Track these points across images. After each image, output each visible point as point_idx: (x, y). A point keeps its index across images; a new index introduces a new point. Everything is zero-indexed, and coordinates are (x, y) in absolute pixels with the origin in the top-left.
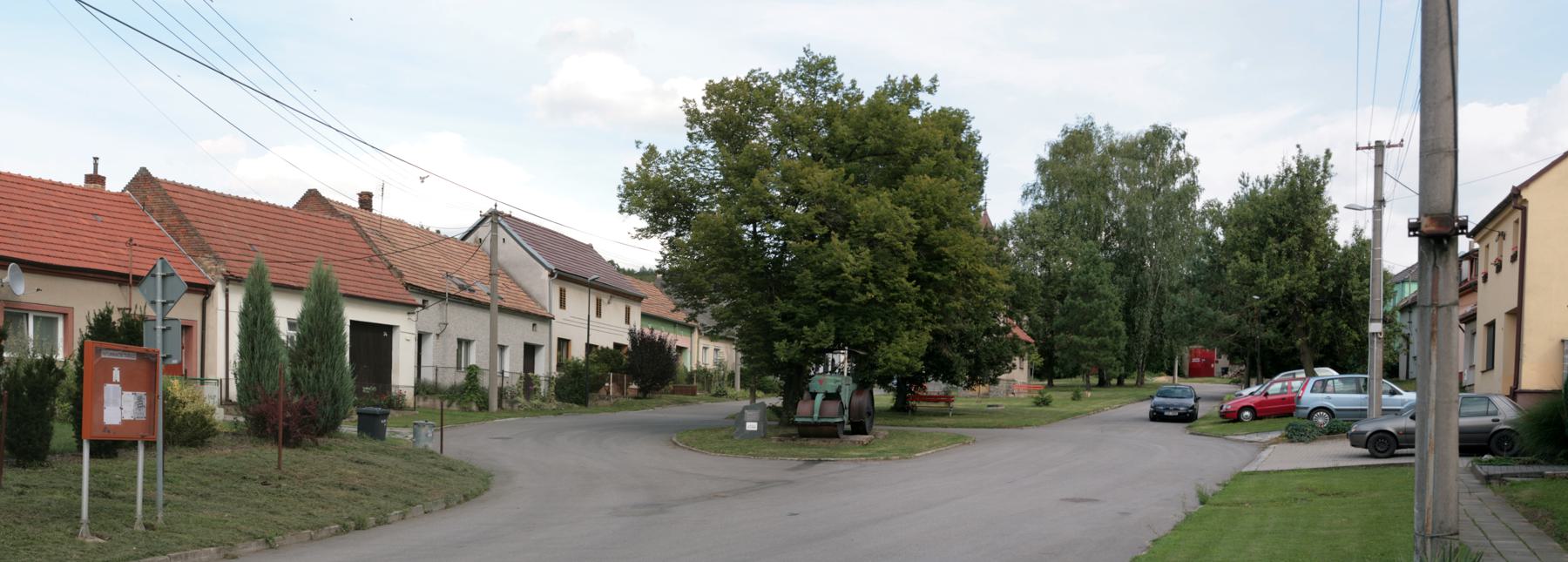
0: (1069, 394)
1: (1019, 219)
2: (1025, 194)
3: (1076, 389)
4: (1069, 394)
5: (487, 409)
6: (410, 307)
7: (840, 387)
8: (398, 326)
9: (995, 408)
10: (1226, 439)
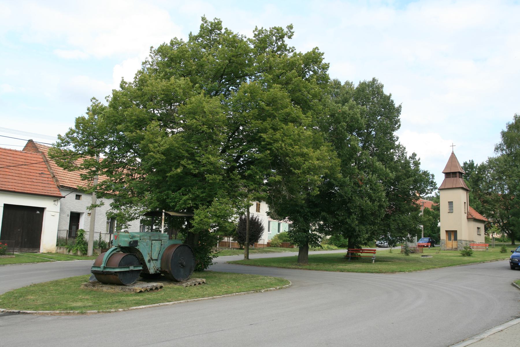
0: (499, 249)
1: (491, 161)
2: (497, 149)
3: (503, 246)
4: (499, 249)
5: (86, 254)
6: (57, 198)
8: (46, 208)
9: (425, 257)
10: (416, 261)
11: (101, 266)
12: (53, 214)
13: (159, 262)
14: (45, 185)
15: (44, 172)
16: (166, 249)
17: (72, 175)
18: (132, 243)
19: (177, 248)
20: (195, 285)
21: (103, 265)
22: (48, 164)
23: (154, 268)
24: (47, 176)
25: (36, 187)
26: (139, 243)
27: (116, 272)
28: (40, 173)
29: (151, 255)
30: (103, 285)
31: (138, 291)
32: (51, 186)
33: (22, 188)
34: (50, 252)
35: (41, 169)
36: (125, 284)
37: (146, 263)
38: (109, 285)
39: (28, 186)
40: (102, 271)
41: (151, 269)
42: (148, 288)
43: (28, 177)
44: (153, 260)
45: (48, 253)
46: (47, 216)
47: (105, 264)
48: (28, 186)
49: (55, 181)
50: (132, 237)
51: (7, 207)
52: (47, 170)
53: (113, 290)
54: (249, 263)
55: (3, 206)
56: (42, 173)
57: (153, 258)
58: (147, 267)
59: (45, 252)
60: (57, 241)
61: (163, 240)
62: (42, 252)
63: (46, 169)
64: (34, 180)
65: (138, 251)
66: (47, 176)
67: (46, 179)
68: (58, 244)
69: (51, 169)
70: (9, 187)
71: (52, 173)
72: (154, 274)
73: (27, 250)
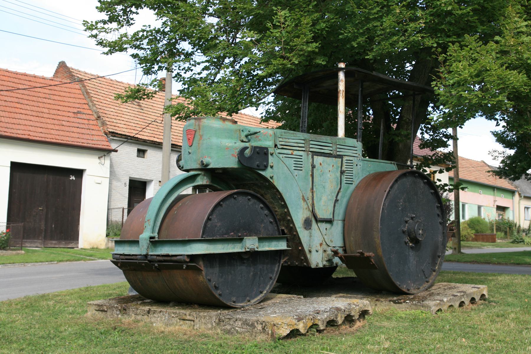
8: (85, 170)
11: (141, 236)
12: (99, 180)
13: (337, 228)
14: (83, 131)
15: (81, 110)
16: (357, 187)
17: (132, 118)
18: (247, 152)
19: (396, 181)
20: (462, 304)
21: (145, 235)
22: (89, 97)
23: (325, 247)
24: (88, 117)
25: (68, 134)
26: (271, 160)
27: (193, 258)
28: (75, 111)
29: (313, 204)
30: (154, 308)
31: (285, 331)
32: (94, 132)
33: (43, 135)
34: (95, 247)
35: (78, 106)
36: (229, 304)
37: (298, 230)
38: (174, 306)
39: (53, 132)
40: (146, 256)
41: (314, 252)
42: (321, 320)
43: (54, 117)
44: (318, 221)
45: (93, 249)
46: (87, 181)
47: (153, 232)
48: (53, 132)
49: (100, 125)
50: (247, 136)
51: (16, 167)
52: (83, 98)
53: (185, 327)
54: (472, 260)
55: (10, 165)
56: (78, 113)
57: (321, 215)
58: (300, 244)
59: (87, 247)
60: (107, 229)
61: (345, 158)
62: (82, 247)
63: (86, 107)
64: (64, 123)
65: (273, 187)
66: (88, 117)
67: (86, 122)
68: (109, 233)
69: (94, 105)
70: (19, 132)
71: (95, 113)
72: (324, 268)
73: (55, 244)
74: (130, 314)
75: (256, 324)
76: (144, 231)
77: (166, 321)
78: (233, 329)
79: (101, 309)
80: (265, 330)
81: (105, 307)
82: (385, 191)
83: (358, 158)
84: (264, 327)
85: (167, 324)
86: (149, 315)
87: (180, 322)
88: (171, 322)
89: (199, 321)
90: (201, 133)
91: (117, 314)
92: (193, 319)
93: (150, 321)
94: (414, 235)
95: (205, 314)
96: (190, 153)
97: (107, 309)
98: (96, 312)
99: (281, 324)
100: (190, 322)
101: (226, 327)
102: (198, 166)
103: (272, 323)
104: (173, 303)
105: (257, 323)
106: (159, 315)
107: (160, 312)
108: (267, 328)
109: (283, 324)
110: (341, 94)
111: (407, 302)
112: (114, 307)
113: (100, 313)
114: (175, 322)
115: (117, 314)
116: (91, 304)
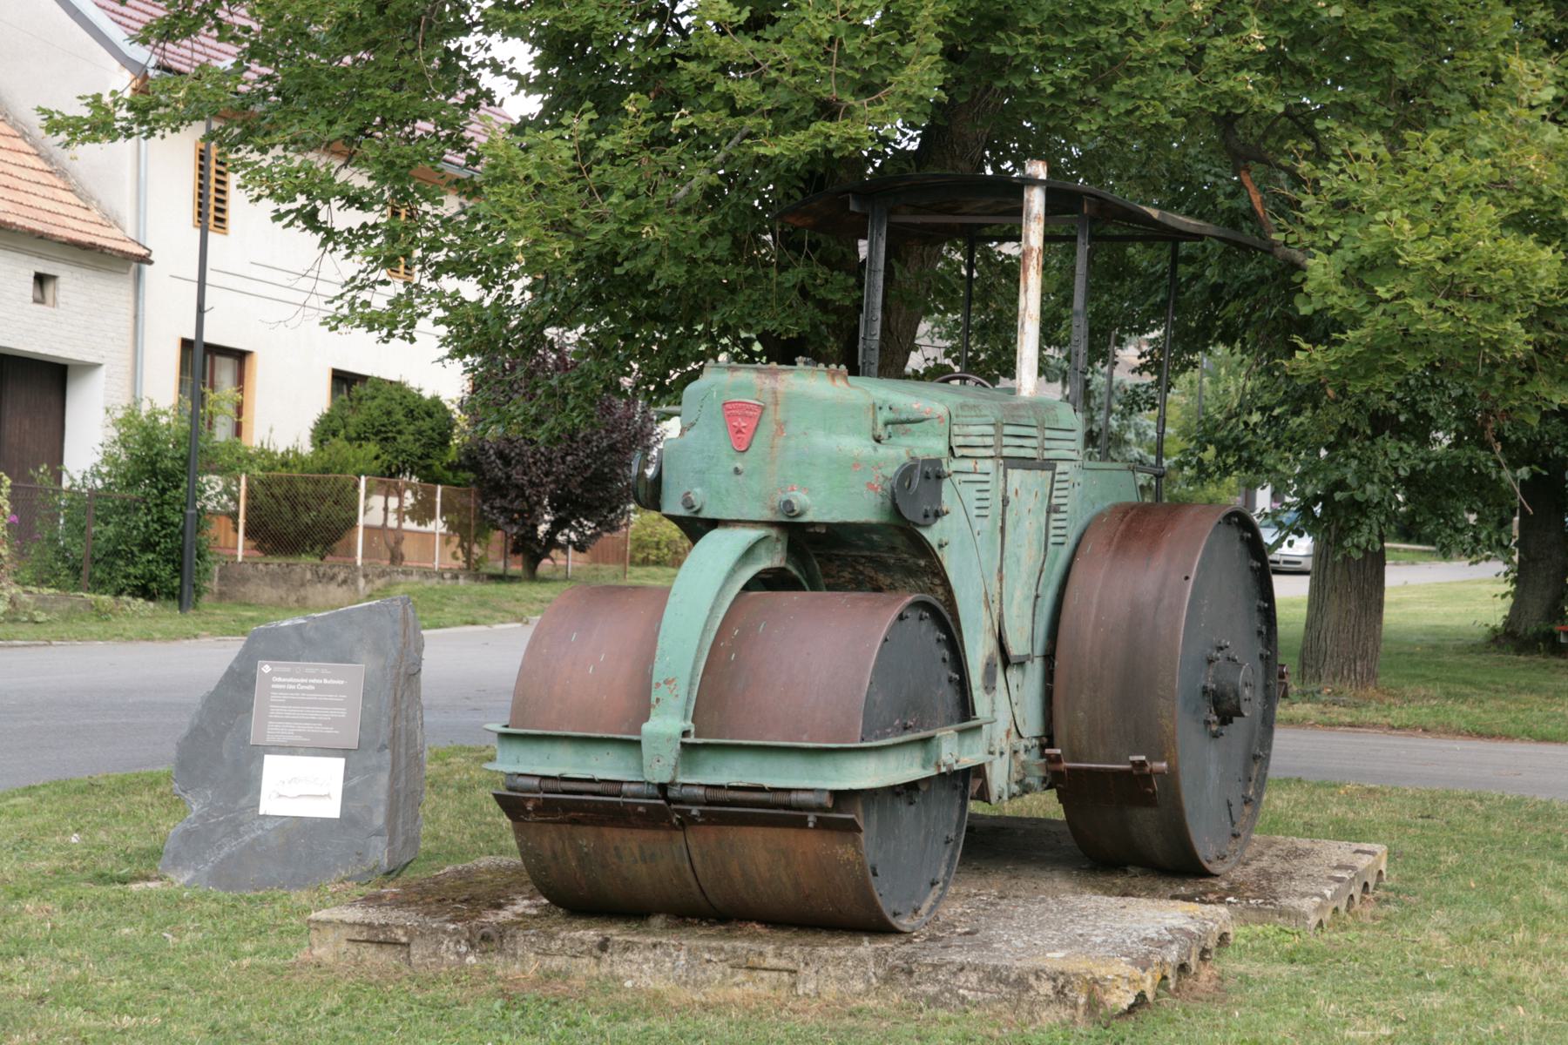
7: (930, 474)
29: (1001, 616)
74: (520, 952)
75: (1032, 980)
76: (653, 712)
77: (679, 971)
78: (947, 995)
79: (382, 937)
80: (1065, 995)
81: (400, 932)
82: (1187, 578)
83: (1077, 463)
84: (1063, 987)
85: (686, 983)
86: (605, 956)
87: (733, 975)
88: (701, 977)
89: (817, 972)
90: (780, 416)
91: (458, 953)
92: (791, 966)
93: (611, 973)
94: (1234, 702)
95: (842, 953)
96: (737, 471)
97: (411, 939)
98: (350, 945)
99: (1113, 980)
100: (775, 974)
101: (923, 987)
102: (768, 515)
103: (1088, 977)
104: (662, 917)
105: (1038, 978)
106: (651, 956)
107: (655, 946)
108: (1071, 991)
109: (1120, 980)
110: (1035, 261)
111: (1230, 903)
112: (445, 932)
113: (373, 949)
114: (719, 976)
115: (458, 953)
116: (329, 922)
